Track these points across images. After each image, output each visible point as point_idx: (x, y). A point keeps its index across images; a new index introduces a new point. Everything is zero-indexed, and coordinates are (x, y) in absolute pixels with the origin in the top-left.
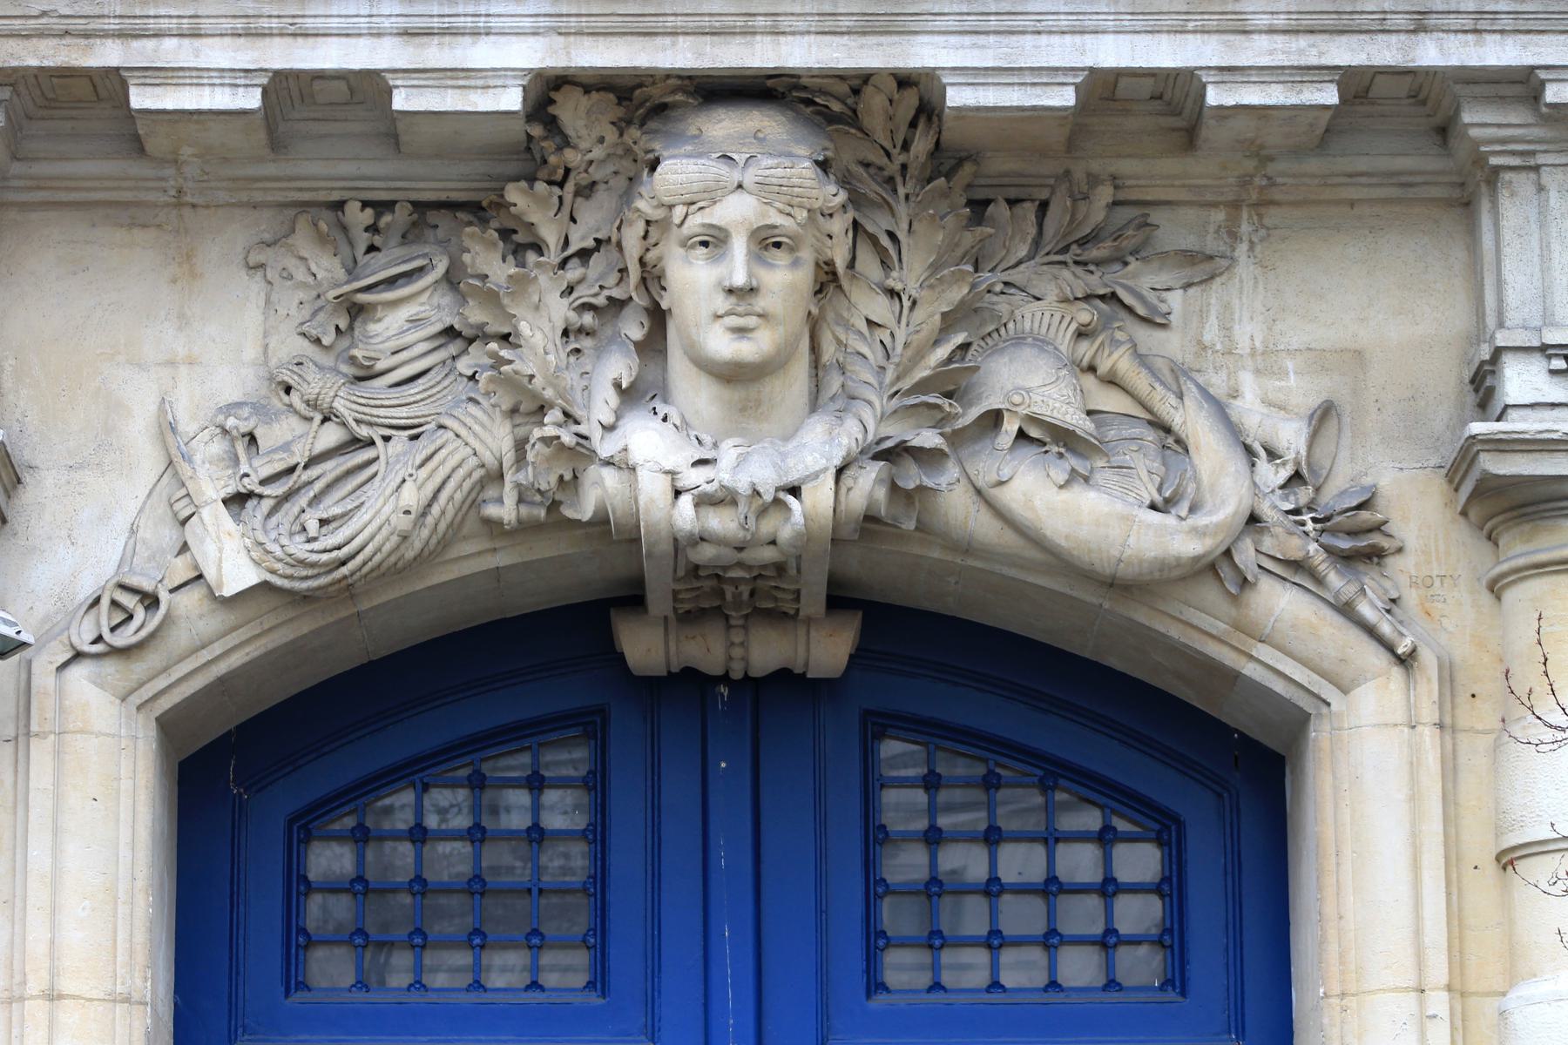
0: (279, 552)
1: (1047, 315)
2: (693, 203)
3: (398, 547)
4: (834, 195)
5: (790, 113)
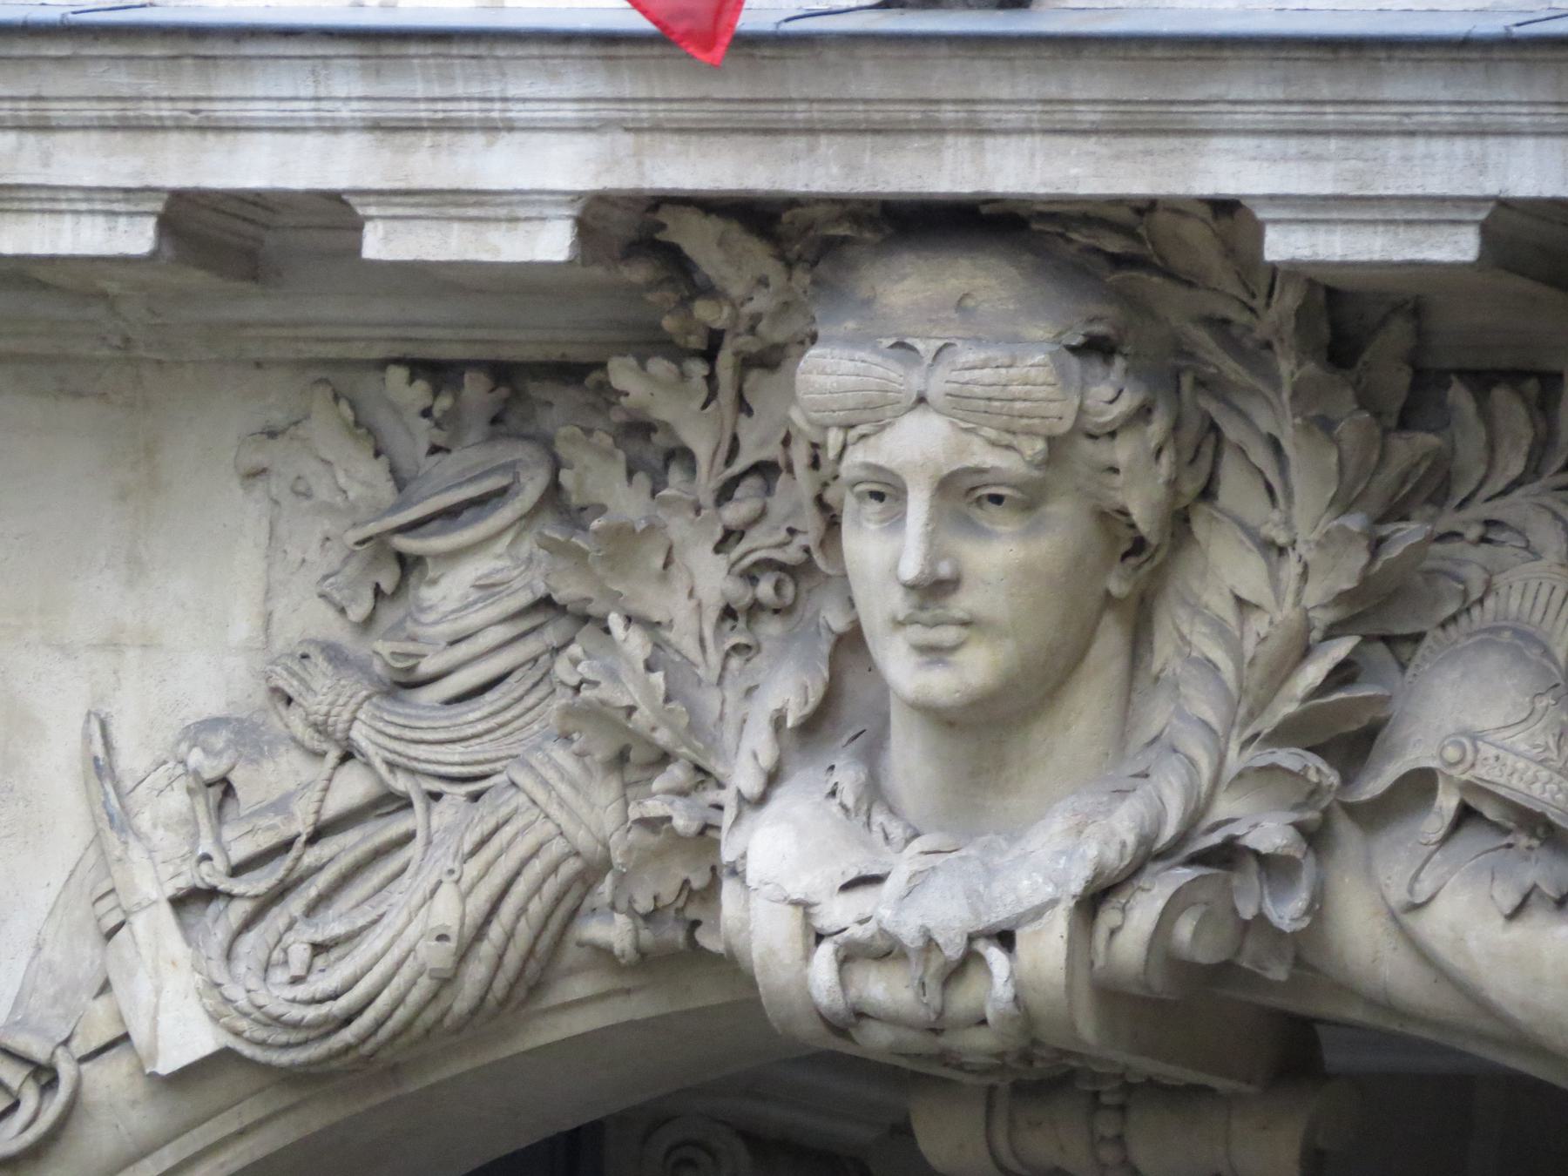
0: (243, 1002)
1: (1545, 590)
2: (852, 427)
3: (435, 996)
4: (1111, 402)
5: (1027, 258)
